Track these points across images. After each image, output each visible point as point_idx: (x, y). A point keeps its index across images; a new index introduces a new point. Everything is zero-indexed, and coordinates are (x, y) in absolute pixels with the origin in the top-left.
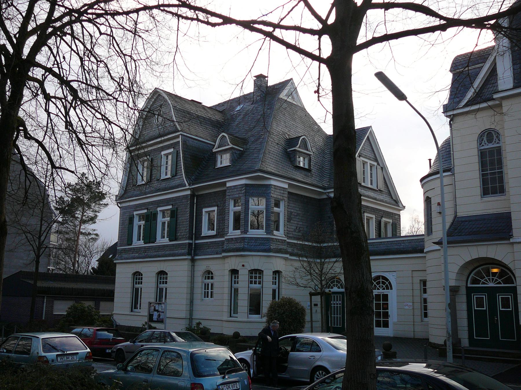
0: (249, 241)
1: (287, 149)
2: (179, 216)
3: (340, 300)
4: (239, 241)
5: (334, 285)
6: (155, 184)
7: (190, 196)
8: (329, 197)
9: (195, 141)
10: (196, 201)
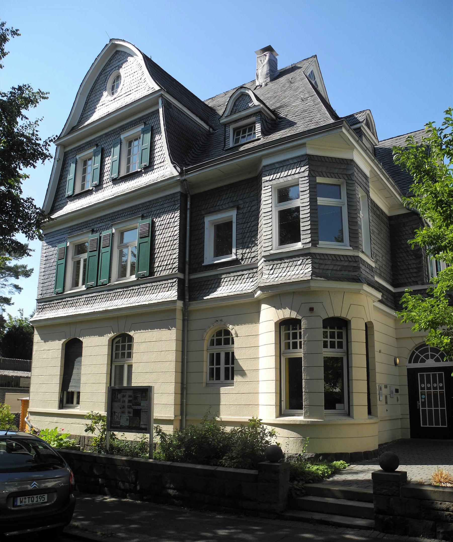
0: (321, 262)
2: (157, 233)
3: (441, 381)
5: (427, 357)
7: (179, 194)
10: (191, 205)
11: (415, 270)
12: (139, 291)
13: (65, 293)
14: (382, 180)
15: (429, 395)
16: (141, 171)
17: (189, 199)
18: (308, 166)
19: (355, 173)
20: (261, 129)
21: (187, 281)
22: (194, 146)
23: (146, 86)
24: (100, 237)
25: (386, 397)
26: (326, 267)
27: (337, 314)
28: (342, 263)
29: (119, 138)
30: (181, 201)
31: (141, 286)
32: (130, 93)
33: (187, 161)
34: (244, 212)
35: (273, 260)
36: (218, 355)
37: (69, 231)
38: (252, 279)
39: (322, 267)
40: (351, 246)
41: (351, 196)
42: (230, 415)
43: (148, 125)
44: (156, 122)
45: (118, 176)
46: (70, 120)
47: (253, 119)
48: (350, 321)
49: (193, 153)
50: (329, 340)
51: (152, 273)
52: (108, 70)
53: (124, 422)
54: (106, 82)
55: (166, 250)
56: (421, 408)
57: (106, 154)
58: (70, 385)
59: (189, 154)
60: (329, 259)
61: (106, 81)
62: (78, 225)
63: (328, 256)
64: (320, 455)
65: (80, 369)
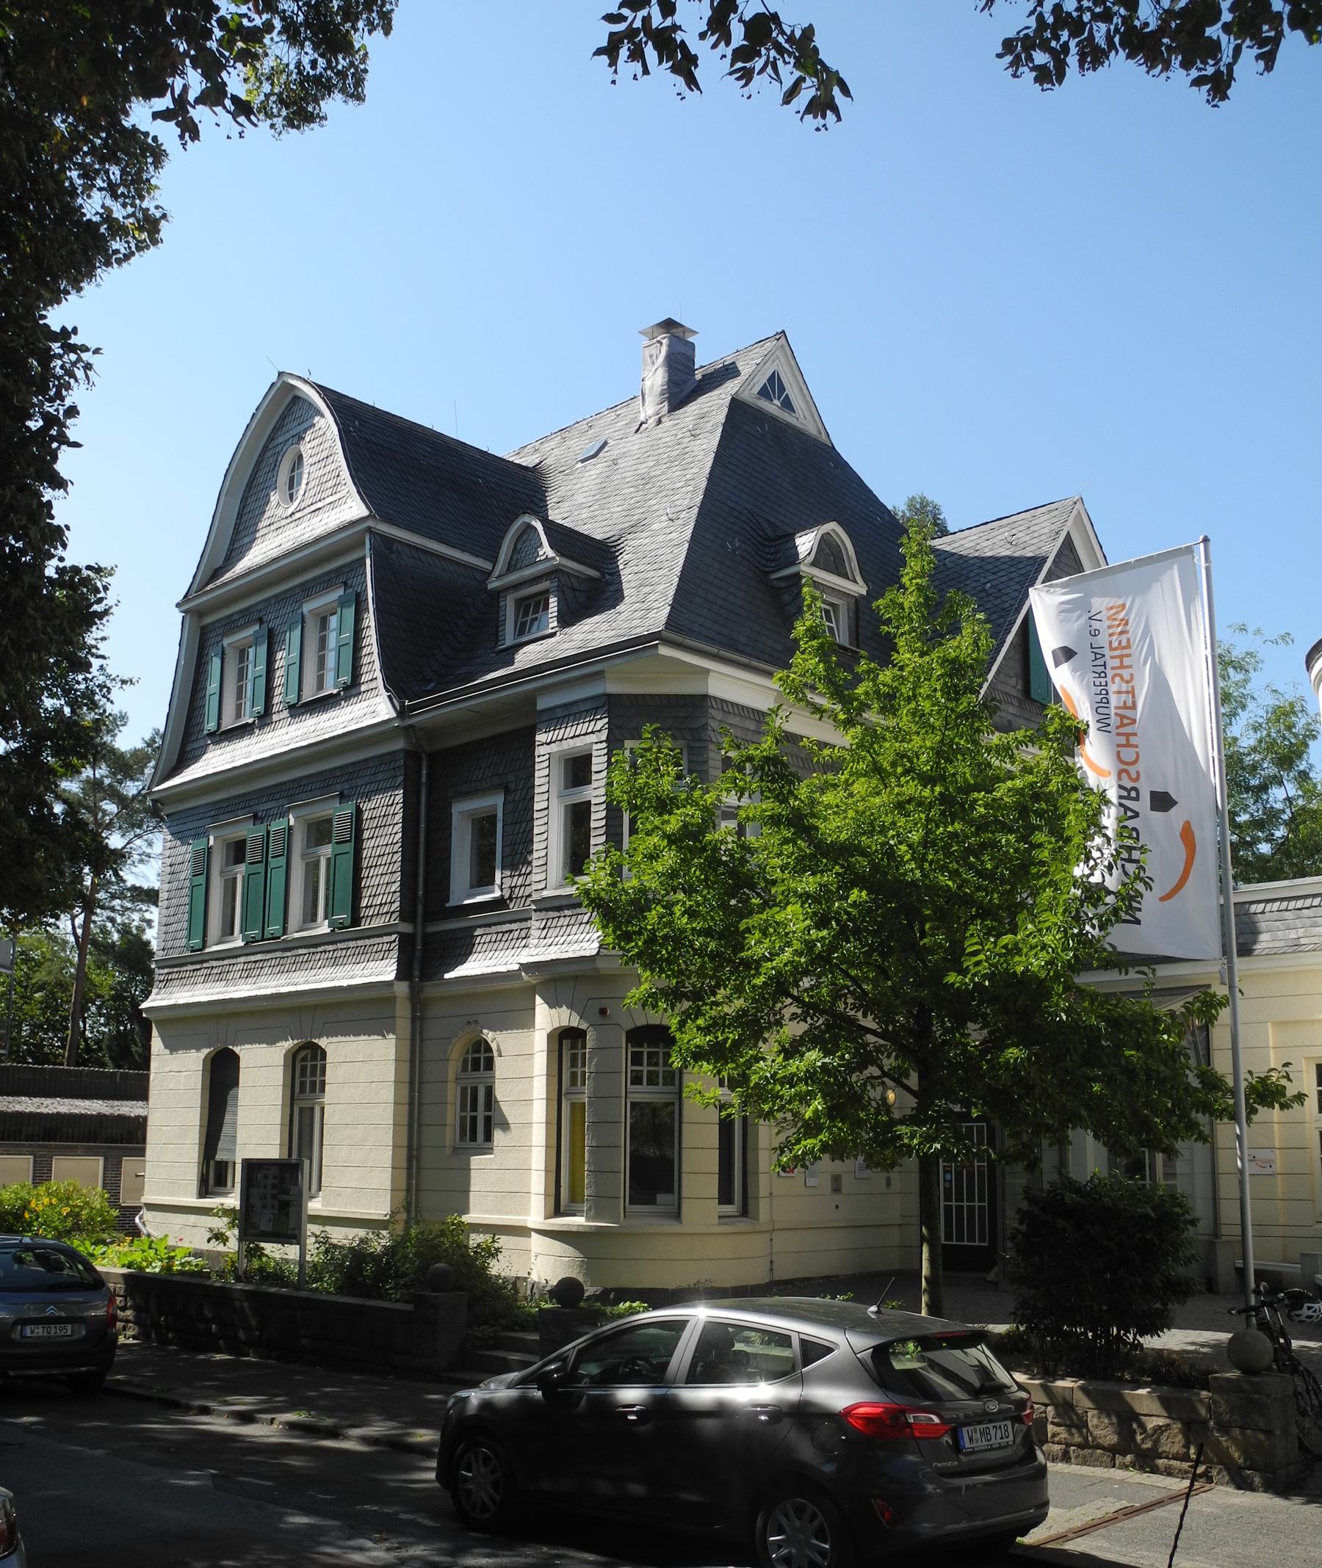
1: (767, 573)
2: (366, 835)
7: (402, 755)
9: (422, 557)
13: (207, 950)
16: (339, 693)
18: (606, 720)
20: (558, 611)
24: (268, 832)
31: (340, 946)
35: (547, 910)
37: (213, 813)
42: (486, 1212)
45: (299, 701)
46: (206, 555)
47: (544, 585)
51: (356, 920)
53: (265, 1226)
58: (219, 1146)
61: (275, 466)
62: (228, 799)
64: (612, 1290)
65: (235, 1113)
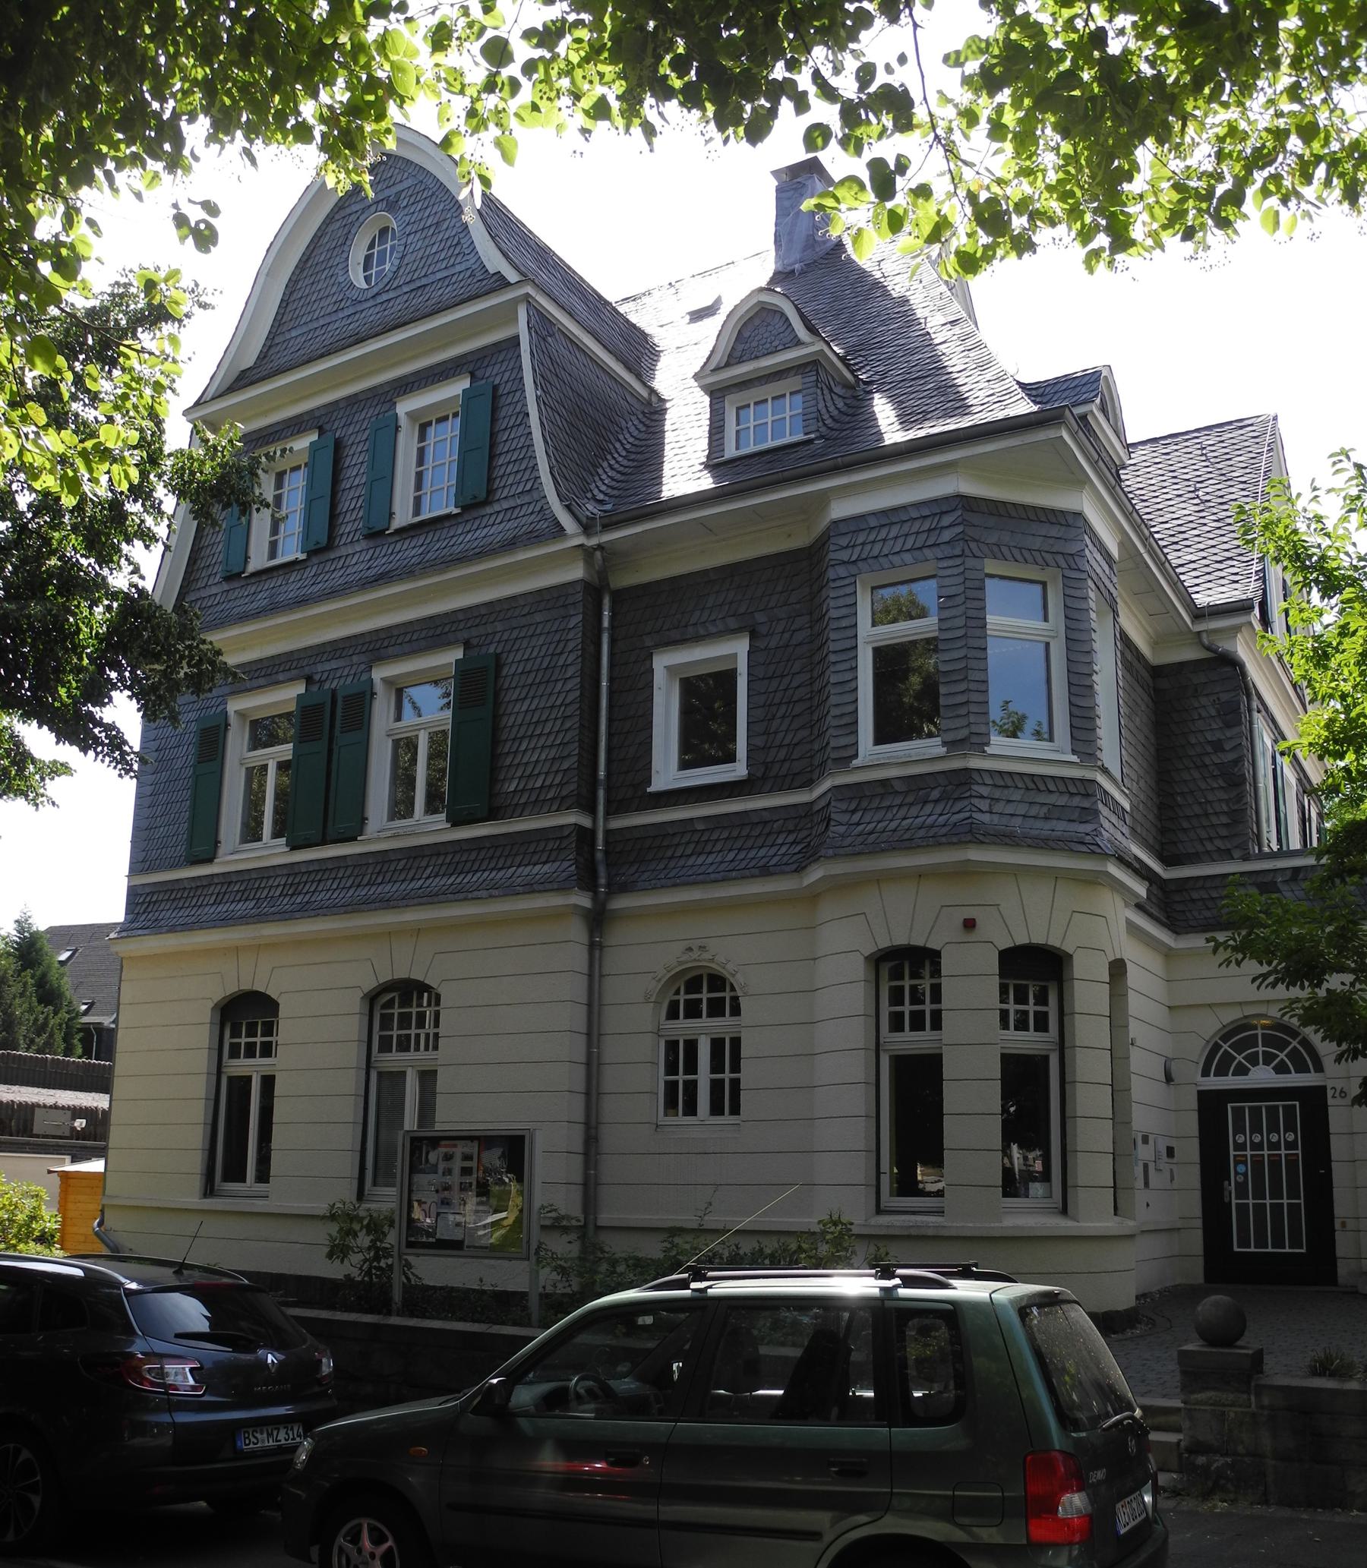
0: (997, 794)
3: (1290, 1127)
4: (935, 794)
5: (1253, 1060)
6: (355, 555)
8: (1215, 651)
10: (612, 618)
11: (1224, 820)
12: (457, 859)
14: (1148, 566)
15: (1258, 1163)
17: (606, 602)
19: (1087, 552)
21: (600, 836)
22: (611, 447)
23: (474, 267)
25: (1146, 1166)
26: (1009, 809)
27: (1038, 939)
28: (1052, 799)
29: (390, 413)
30: (584, 606)
32: (424, 281)
33: (596, 492)
34: (773, 644)
36: (692, 1046)
38: (795, 835)
39: (999, 807)
40: (1074, 752)
41: (1076, 615)
43: (484, 381)
44: (507, 374)
48: (1070, 956)
49: (610, 466)
50: (1012, 1007)
52: (354, 208)
54: (348, 243)
55: (540, 745)
56: (1234, 1201)
57: (349, 459)
59: (600, 471)
60: (1016, 787)
63: (1015, 777)
